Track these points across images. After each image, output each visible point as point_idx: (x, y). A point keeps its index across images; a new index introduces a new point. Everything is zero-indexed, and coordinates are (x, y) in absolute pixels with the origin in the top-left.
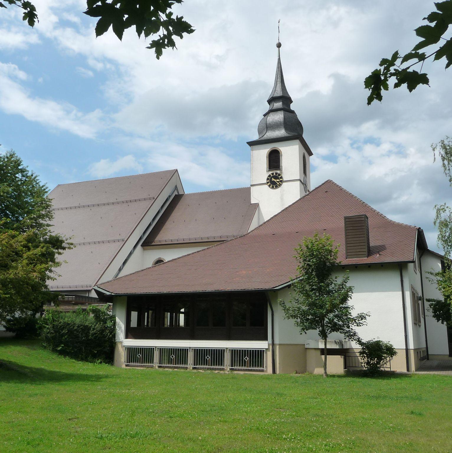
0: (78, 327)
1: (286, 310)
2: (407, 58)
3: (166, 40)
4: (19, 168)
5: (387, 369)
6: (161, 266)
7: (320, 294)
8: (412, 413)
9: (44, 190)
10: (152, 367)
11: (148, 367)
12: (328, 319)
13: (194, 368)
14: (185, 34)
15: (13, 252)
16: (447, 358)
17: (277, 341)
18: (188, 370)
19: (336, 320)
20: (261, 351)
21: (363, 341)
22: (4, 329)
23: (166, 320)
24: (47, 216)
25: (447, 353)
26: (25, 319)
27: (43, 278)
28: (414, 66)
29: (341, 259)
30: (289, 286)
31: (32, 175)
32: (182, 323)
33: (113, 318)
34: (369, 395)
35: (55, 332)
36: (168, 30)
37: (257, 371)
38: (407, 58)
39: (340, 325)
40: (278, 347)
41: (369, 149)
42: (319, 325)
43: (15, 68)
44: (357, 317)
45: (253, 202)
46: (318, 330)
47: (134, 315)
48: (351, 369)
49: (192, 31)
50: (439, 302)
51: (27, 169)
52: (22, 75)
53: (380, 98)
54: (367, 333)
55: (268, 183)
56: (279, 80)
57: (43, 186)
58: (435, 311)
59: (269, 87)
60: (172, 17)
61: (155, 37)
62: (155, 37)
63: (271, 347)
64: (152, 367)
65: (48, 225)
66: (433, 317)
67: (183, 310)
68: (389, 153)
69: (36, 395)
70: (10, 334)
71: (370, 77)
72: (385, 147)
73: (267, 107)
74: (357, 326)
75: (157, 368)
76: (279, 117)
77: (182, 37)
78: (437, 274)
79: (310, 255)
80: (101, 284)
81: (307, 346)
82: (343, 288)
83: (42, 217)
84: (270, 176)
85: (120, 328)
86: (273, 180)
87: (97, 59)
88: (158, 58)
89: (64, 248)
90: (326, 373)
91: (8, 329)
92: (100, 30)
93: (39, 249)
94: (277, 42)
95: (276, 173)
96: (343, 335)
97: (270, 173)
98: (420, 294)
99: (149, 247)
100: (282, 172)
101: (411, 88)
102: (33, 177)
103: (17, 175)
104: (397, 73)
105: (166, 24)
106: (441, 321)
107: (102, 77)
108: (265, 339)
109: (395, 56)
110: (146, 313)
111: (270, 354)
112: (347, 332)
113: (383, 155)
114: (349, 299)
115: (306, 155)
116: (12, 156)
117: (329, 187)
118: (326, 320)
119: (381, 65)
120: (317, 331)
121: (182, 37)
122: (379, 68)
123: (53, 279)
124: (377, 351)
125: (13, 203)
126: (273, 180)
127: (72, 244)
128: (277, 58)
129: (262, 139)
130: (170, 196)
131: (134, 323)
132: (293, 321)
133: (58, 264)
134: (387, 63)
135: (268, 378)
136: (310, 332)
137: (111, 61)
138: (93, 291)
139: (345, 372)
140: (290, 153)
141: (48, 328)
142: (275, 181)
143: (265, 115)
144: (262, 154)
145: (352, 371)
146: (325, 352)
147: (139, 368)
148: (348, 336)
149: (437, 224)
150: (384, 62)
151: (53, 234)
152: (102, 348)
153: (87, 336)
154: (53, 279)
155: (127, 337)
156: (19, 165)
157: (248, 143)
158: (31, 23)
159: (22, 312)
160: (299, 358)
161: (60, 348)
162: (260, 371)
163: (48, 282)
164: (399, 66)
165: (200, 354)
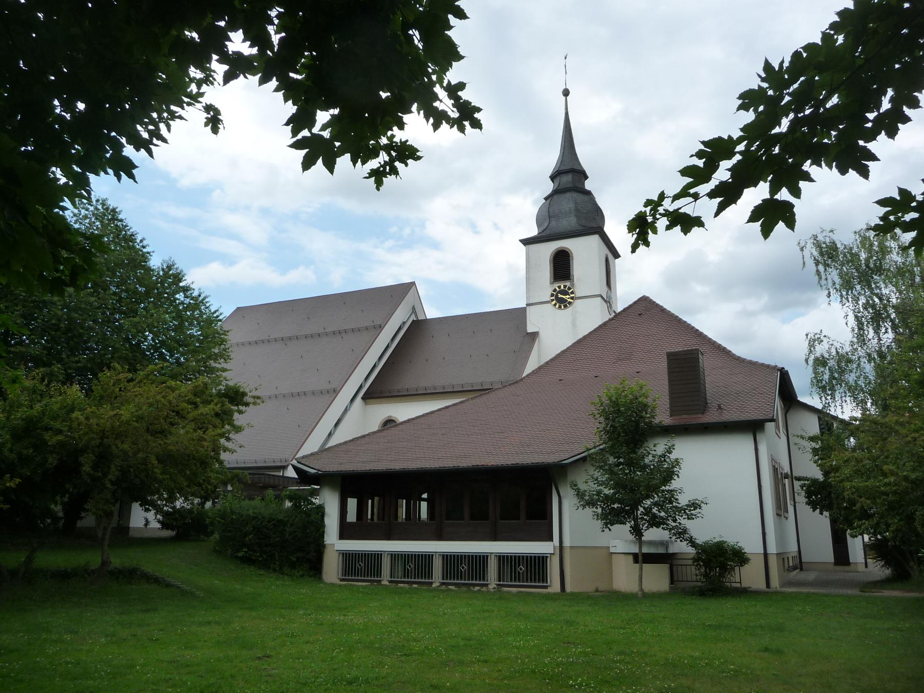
0: (269, 522)
1: (580, 495)
2: (676, 197)
3: (388, 168)
4: (181, 284)
5: (734, 585)
6: (393, 431)
7: (630, 471)
8: (766, 650)
9: (218, 316)
12: (644, 508)
13: (443, 584)
14: (410, 161)
15: (173, 411)
16: (832, 567)
17: (567, 543)
19: (655, 510)
21: (697, 541)
23: (400, 510)
24: (222, 356)
25: (833, 561)
26: (190, 511)
27: (217, 449)
28: (687, 206)
29: (663, 417)
30: (584, 459)
31: (199, 296)
32: (424, 514)
34: (704, 624)
36: (389, 154)
38: (676, 197)
39: (662, 518)
42: (629, 517)
44: (687, 505)
46: (628, 525)
47: (352, 503)
48: (681, 585)
49: (419, 158)
50: (814, 481)
51: (192, 286)
53: (647, 244)
54: (704, 530)
57: (215, 312)
58: (809, 495)
60: (395, 140)
61: (374, 164)
62: (374, 164)
65: (225, 370)
66: (807, 503)
67: (425, 496)
69: (209, 623)
70: (168, 533)
71: (633, 219)
73: (549, 187)
74: (688, 519)
77: (406, 165)
78: (812, 439)
79: (614, 412)
80: (303, 457)
81: (612, 550)
82: (665, 461)
83: (216, 357)
84: (555, 290)
86: (560, 296)
88: (378, 189)
89: (247, 404)
91: (165, 525)
92: (307, 164)
93: (211, 406)
96: (667, 532)
98: (787, 469)
100: (573, 285)
101: (686, 230)
102: (200, 299)
103: (177, 296)
104: (667, 214)
105: (388, 148)
106: (818, 510)
108: (550, 539)
109: (662, 196)
110: (370, 501)
112: (673, 528)
114: (675, 477)
115: (611, 257)
116: (169, 267)
117: (645, 306)
118: (641, 509)
119: (645, 206)
120: (627, 527)
121: (406, 165)
122: (643, 209)
123: (232, 451)
124: (720, 559)
125: (172, 338)
126: (560, 296)
127: (258, 398)
131: (352, 517)
132: (589, 511)
133: (238, 429)
134: (654, 205)
135: (552, 597)
136: (616, 528)
138: (290, 468)
139: (670, 588)
145: (678, 587)
146: (640, 558)
147: (360, 584)
148: (674, 534)
149: (811, 362)
150: (648, 203)
151: (231, 383)
152: (304, 554)
154: (232, 451)
156: (180, 280)
157: (521, 241)
158: (215, 130)
159: (186, 499)
161: (240, 554)
163: (224, 456)
164: (668, 205)
165: (452, 561)
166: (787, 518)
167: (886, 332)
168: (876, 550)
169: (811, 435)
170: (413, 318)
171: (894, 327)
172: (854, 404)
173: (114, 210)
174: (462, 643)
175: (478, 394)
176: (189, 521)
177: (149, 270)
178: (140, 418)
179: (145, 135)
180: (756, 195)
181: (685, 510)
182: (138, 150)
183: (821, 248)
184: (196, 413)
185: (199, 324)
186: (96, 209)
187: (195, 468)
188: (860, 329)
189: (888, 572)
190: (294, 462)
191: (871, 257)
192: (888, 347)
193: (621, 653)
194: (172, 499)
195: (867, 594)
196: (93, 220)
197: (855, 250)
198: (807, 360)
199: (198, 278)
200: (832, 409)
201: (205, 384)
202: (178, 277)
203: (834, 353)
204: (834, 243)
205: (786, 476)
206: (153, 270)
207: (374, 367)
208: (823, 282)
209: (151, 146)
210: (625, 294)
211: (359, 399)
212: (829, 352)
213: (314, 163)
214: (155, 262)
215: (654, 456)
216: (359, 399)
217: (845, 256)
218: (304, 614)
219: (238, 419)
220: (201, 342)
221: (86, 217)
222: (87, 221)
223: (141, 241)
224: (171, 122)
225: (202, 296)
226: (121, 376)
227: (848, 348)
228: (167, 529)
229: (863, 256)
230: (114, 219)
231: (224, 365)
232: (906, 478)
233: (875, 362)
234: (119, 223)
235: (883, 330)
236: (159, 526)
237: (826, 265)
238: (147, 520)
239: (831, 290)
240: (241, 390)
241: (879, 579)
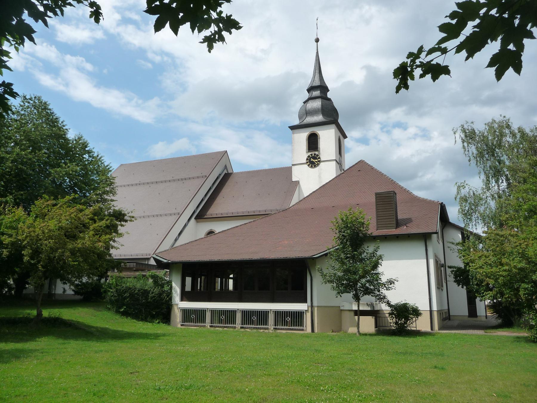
0: (139, 291)
1: (324, 276)
2: (431, 51)
3: (217, 36)
4: (86, 149)
5: (413, 329)
6: (212, 237)
7: (353, 262)
8: (436, 367)
9: (109, 169)
12: (361, 283)
13: (242, 328)
15: (81, 224)
17: (315, 304)
19: (367, 285)
21: (392, 303)
24: (111, 192)
26: (91, 284)
28: (437, 59)
29: (373, 230)
30: (326, 255)
31: (98, 156)
32: (231, 287)
33: (169, 283)
36: (218, 26)
37: (295, 330)
38: (431, 51)
39: (371, 289)
40: (316, 309)
42: (352, 289)
43: (82, 61)
47: (189, 280)
48: (381, 328)
49: (240, 28)
50: (459, 269)
51: (93, 150)
52: (89, 67)
53: (407, 87)
54: (395, 296)
55: (307, 162)
56: (317, 71)
57: (107, 166)
60: (222, 15)
61: (207, 33)
62: (207, 33)
63: (310, 308)
64: (205, 326)
65: (112, 201)
66: (455, 282)
67: (231, 276)
71: (398, 68)
72: (412, 131)
73: (307, 95)
76: (317, 104)
77: (231, 33)
78: (458, 244)
81: (342, 308)
82: (374, 256)
83: (107, 193)
84: (309, 156)
87: (155, 53)
89: (126, 221)
90: (359, 331)
91: (76, 293)
93: (104, 221)
94: (316, 37)
95: (315, 154)
96: (374, 298)
97: (309, 154)
98: (443, 262)
101: (435, 78)
102: (99, 158)
103: (84, 156)
104: (422, 65)
105: (217, 22)
106: (461, 286)
107: (160, 68)
108: (305, 301)
109: (421, 50)
111: (309, 315)
112: (378, 296)
113: (409, 138)
114: (380, 266)
115: (342, 138)
116: (80, 139)
118: (359, 284)
119: (408, 58)
120: (351, 295)
121: (231, 33)
124: (404, 312)
125: (81, 181)
127: (133, 217)
128: (316, 51)
129: (302, 123)
130: (220, 175)
131: (188, 288)
132: (329, 285)
133: (121, 235)
134: (413, 56)
135: (307, 336)
136: (345, 295)
137: (168, 54)
139: (376, 331)
140: (327, 137)
141: (112, 292)
142: (313, 162)
143: (304, 103)
144: (302, 136)
145: (382, 330)
146: (358, 313)
148: (378, 299)
149: (458, 200)
150: (410, 55)
151: (117, 208)
152: (161, 310)
153: (147, 298)
154: (117, 248)
155: (182, 300)
156: (86, 147)
157: (289, 127)
158: (97, 20)
159: (89, 277)
160: (335, 319)
163: (112, 251)
164: (424, 58)
166: (442, 290)
167: (502, 182)
168: (494, 307)
169: (458, 242)
170: (225, 172)
171: (507, 180)
172: (483, 224)
173: (45, 103)
174: (254, 364)
175: (264, 216)
176: (90, 290)
177: (67, 140)
178: (61, 228)
179: (41, 9)
180: (493, 47)
181: (385, 285)
182: (37, 21)
183: (466, 133)
184: (95, 225)
185: (97, 173)
186: (34, 102)
187: (101, 262)
188: (488, 180)
189: (500, 321)
190: (155, 256)
191: (495, 138)
192: (503, 191)
193: (351, 370)
194: (80, 277)
195: (489, 334)
196: (33, 109)
197: (486, 134)
198: (456, 198)
200: (470, 227)
201: (101, 209)
202: (85, 145)
203: (472, 194)
204: (473, 129)
205: (442, 266)
206: (69, 140)
207: (202, 200)
208: (467, 153)
209: (46, 18)
210: (349, 161)
211: (193, 219)
212: (469, 193)
213: (163, 27)
214: (71, 135)
215: (367, 253)
216: (193, 219)
217: (480, 137)
218: (160, 346)
219: (121, 229)
220: (98, 184)
221: (28, 107)
222: (29, 109)
223: (62, 122)
224: (64, 8)
225: (99, 156)
226: (49, 202)
227: (480, 192)
228: (78, 295)
229: (490, 138)
230: (45, 109)
231: (113, 198)
232: (515, 267)
233: (495, 200)
234: (49, 111)
235: (501, 181)
236: (73, 293)
237: (469, 143)
238: (64, 289)
239: (471, 157)
240: (123, 212)
241: (495, 325)
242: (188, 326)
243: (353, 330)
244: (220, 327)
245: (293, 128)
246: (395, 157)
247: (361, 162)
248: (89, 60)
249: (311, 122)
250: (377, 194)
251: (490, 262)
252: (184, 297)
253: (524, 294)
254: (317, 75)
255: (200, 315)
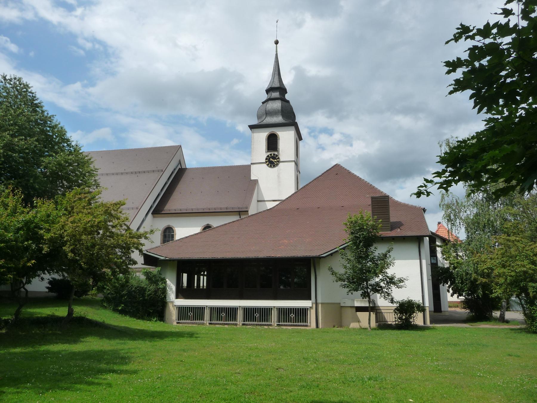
0: (136, 288)
6: (209, 232)
10: (203, 324)
11: (199, 324)
13: (243, 324)
17: (319, 301)
18: (238, 326)
20: (305, 309)
22: (47, 290)
33: (164, 281)
35: (116, 292)
37: (301, 326)
40: (320, 305)
41: (324, 139)
43: (7, 41)
45: (253, 178)
52: (13, 48)
54: (400, 295)
55: (266, 162)
56: (277, 73)
59: (265, 78)
63: (314, 305)
64: (203, 324)
68: (339, 142)
72: (337, 136)
73: (265, 97)
75: (208, 324)
76: (277, 105)
81: (342, 305)
84: (268, 156)
85: (171, 289)
86: (271, 160)
87: (87, 39)
90: (370, 326)
94: (275, 39)
95: (274, 154)
97: (269, 153)
99: (159, 215)
107: (91, 56)
108: (309, 298)
111: (313, 311)
113: (334, 144)
124: (406, 308)
126: (271, 160)
128: (275, 53)
129: (262, 123)
130: (175, 169)
137: (100, 42)
140: (286, 137)
141: (108, 290)
142: (272, 161)
143: (263, 103)
144: (262, 136)
152: (155, 307)
153: (143, 295)
155: (177, 297)
157: (249, 126)
160: (337, 315)
161: (120, 308)
162: (303, 326)
170: (179, 167)
199: (75, 137)
211: (150, 214)
216: (150, 214)
242: (184, 323)
243: (354, 325)
244: (220, 324)
245: (252, 127)
246: (315, 160)
247: (337, 166)
248: (14, 41)
249: (271, 123)
250: (373, 198)
251: (495, 264)
252: (180, 295)
253: (533, 292)
254: (277, 77)
255: (198, 313)
